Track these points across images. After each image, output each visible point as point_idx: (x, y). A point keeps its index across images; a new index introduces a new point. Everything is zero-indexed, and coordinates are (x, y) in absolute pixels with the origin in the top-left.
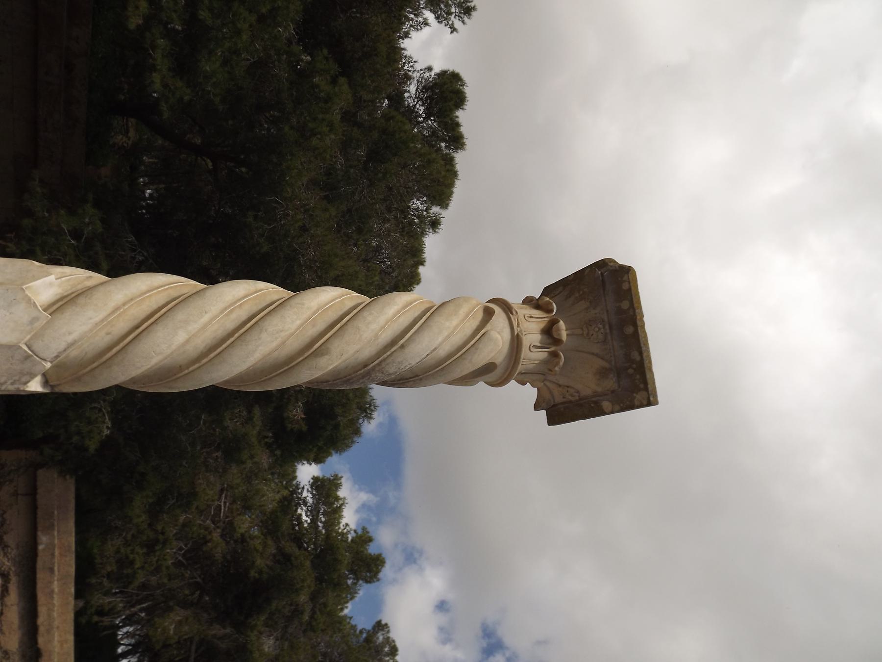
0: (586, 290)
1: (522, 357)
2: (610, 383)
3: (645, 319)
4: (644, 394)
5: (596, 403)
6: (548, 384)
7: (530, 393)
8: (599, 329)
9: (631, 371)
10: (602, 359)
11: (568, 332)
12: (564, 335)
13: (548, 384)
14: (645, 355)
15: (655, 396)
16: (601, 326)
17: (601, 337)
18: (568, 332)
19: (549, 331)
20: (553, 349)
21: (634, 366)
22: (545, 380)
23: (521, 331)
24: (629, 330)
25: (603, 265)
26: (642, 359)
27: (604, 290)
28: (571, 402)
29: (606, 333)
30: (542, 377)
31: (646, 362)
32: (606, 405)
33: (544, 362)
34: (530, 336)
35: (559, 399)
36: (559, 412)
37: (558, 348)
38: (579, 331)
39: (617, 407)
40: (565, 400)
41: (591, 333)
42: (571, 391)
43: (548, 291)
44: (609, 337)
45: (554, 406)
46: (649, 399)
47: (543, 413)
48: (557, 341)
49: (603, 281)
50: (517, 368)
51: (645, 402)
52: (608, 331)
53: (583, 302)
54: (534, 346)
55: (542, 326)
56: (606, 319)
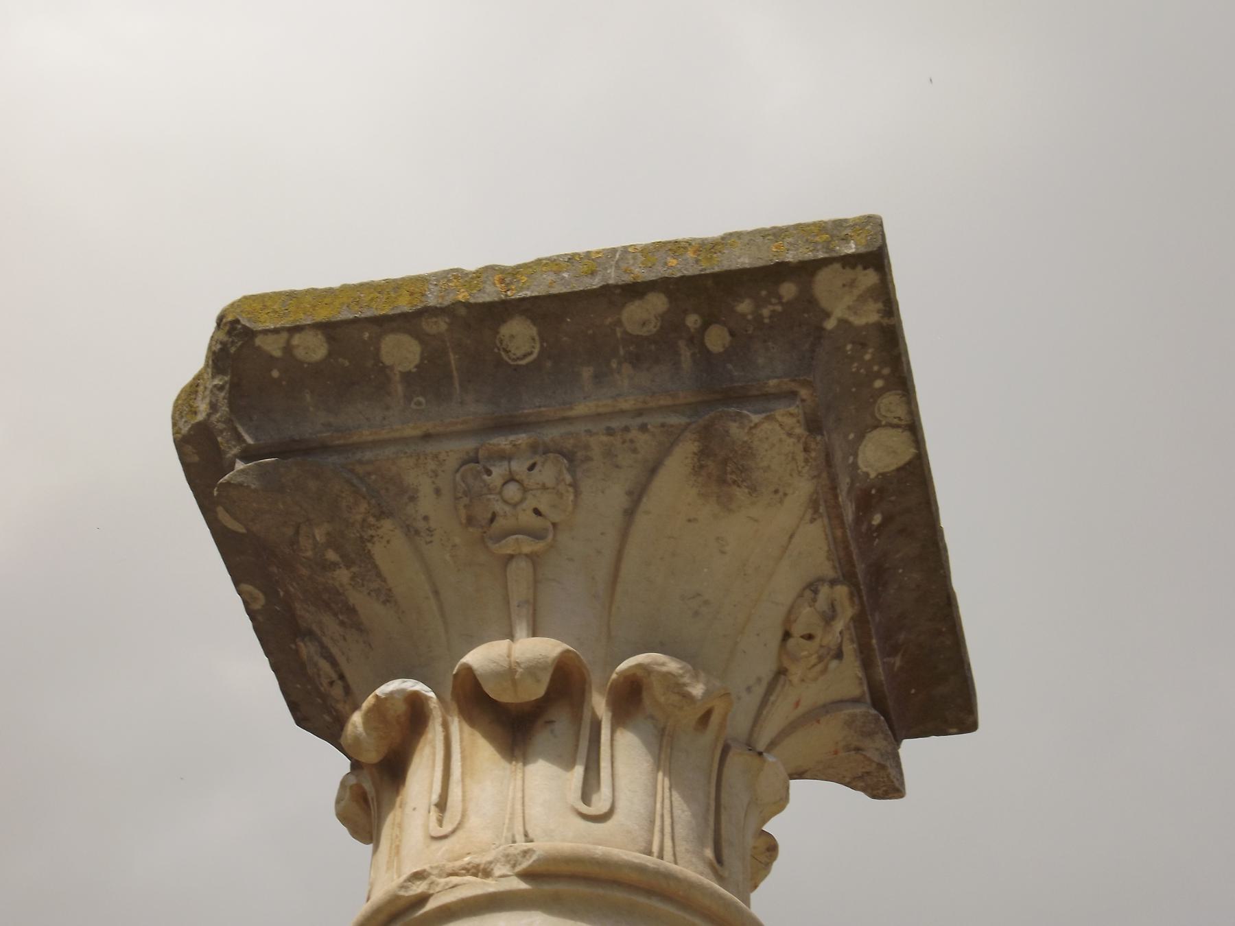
0: (320, 534)
1: (634, 856)
2: (773, 436)
3: (471, 264)
4: (826, 285)
5: (865, 503)
6: (780, 714)
7: (816, 816)
8: (511, 479)
9: (717, 339)
10: (653, 471)
11: (521, 629)
12: (534, 648)
13: (780, 714)
14: (641, 273)
15: (837, 229)
16: (498, 471)
17: (547, 473)
18: (521, 629)
19: (516, 723)
20: (599, 704)
21: (693, 321)
22: (750, 746)
23: (511, 860)
24: (520, 337)
25: (200, 452)
26: (665, 285)
27: (325, 448)
28: (860, 621)
29: (534, 448)
30: (737, 760)
31: (676, 267)
32: (877, 455)
33: (665, 749)
34: (536, 812)
35: (846, 678)
36: (914, 676)
37: (595, 677)
38: (520, 569)
39: (889, 405)
40: (849, 648)
41: (526, 518)
42: (807, 617)
43: (315, 707)
44: (551, 434)
45: (878, 701)
46: (849, 261)
47: (917, 754)
48: (566, 683)
49: (285, 450)
50: (692, 885)
51: (869, 278)
52: (522, 438)
53: (377, 550)
54: (588, 790)
55: (485, 752)
56: (469, 445)
